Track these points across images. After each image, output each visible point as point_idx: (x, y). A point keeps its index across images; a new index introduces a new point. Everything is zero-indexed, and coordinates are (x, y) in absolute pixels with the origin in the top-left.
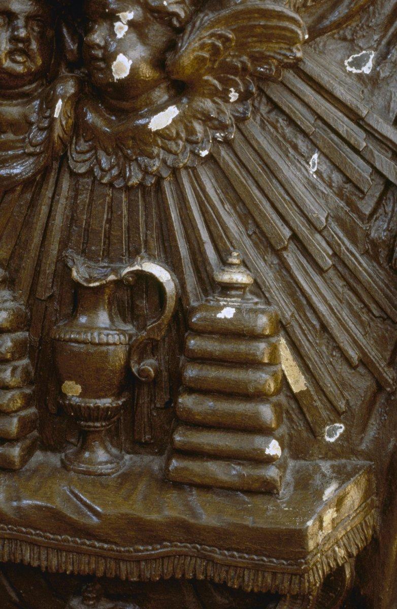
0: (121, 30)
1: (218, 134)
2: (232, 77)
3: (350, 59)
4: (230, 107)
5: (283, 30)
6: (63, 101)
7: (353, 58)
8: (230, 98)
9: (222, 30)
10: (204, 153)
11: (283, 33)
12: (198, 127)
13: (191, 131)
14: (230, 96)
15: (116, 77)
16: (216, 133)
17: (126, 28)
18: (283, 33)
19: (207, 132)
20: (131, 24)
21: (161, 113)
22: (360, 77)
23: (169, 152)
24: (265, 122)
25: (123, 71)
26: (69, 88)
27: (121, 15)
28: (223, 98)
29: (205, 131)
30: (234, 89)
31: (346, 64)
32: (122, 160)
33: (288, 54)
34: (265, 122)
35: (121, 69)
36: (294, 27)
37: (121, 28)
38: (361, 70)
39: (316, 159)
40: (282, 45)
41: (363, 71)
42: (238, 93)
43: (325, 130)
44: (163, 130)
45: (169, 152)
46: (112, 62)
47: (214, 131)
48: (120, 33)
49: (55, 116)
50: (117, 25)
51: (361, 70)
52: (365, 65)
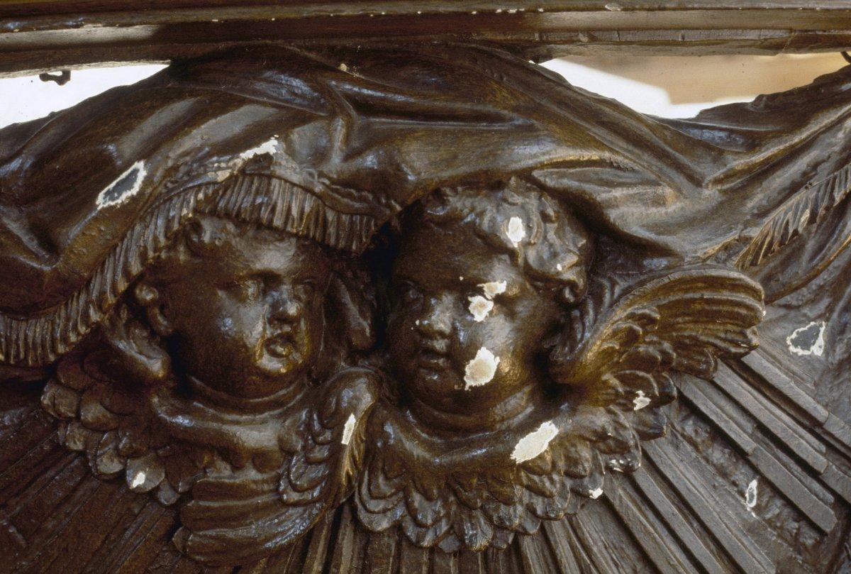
0: (481, 308)
1: (614, 462)
2: (641, 374)
3: (794, 336)
4: (631, 416)
5: (736, 306)
6: (356, 417)
7: (798, 333)
8: (635, 405)
9: (644, 308)
10: (597, 493)
11: (736, 309)
12: (585, 453)
13: (573, 461)
14: (634, 401)
15: (470, 383)
16: (611, 459)
17: (490, 305)
18: (736, 309)
19: (598, 459)
20: (499, 300)
21: (532, 434)
22: (809, 361)
23: (541, 493)
24: (679, 436)
25: (484, 374)
26: (362, 395)
27: (485, 286)
28: (624, 405)
29: (595, 458)
30: (644, 392)
31: (789, 342)
32: (454, 508)
33: (739, 338)
34: (679, 436)
35: (479, 371)
36: (750, 301)
37: (482, 306)
38: (809, 350)
39: (755, 489)
40: (729, 327)
41: (813, 352)
42: (650, 398)
43: (767, 445)
44: (533, 461)
45: (541, 493)
46: (468, 361)
47: (608, 457)
48: (480, 313)
49: (343, 442)
50: (476, 300)
51: (809, 350)
52: (814, 343)
